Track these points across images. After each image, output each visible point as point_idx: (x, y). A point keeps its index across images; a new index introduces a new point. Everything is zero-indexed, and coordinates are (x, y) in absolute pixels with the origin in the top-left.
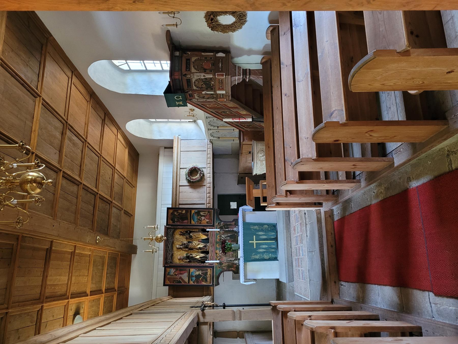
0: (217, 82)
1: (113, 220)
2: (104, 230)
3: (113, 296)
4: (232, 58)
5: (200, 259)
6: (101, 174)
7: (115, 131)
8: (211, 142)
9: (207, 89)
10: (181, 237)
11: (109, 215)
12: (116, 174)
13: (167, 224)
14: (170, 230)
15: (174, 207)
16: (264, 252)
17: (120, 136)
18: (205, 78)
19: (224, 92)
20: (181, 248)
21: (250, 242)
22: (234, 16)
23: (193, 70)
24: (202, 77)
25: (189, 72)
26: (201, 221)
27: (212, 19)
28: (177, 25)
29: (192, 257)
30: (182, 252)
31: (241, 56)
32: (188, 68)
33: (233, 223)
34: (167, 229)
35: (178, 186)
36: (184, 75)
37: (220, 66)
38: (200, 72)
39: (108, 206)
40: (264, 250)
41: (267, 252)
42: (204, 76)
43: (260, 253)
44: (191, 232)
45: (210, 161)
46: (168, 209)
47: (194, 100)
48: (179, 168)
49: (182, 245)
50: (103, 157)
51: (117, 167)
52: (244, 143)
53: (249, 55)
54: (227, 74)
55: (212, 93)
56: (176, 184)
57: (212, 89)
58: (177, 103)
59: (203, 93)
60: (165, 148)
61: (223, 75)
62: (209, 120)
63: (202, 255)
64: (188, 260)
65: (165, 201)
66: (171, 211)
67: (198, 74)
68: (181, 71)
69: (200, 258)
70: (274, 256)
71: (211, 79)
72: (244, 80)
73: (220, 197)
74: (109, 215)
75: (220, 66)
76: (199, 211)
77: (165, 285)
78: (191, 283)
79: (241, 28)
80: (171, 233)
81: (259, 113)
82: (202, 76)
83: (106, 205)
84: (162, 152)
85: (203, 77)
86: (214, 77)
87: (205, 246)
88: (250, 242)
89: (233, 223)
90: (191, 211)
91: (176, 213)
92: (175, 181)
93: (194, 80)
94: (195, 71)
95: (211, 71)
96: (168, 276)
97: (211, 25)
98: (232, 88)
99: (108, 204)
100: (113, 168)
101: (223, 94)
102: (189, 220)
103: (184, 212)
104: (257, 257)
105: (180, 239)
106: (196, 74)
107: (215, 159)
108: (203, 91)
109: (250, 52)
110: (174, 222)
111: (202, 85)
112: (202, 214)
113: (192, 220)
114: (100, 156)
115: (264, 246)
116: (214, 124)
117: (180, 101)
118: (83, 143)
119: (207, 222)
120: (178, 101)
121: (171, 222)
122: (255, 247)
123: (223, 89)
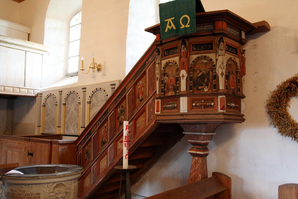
9: (189, 79)
42: (183, 76)
45: (8, 91)
58: (169, 20)
59: (183, 72)
62: (57, 95)
71: (216, 86)
82: (220, 71)
93: (212, 56)
95: (227, 87)
101: (178, 107)
108: (188, 72)
116: (70, 99)
120: (176, 22)
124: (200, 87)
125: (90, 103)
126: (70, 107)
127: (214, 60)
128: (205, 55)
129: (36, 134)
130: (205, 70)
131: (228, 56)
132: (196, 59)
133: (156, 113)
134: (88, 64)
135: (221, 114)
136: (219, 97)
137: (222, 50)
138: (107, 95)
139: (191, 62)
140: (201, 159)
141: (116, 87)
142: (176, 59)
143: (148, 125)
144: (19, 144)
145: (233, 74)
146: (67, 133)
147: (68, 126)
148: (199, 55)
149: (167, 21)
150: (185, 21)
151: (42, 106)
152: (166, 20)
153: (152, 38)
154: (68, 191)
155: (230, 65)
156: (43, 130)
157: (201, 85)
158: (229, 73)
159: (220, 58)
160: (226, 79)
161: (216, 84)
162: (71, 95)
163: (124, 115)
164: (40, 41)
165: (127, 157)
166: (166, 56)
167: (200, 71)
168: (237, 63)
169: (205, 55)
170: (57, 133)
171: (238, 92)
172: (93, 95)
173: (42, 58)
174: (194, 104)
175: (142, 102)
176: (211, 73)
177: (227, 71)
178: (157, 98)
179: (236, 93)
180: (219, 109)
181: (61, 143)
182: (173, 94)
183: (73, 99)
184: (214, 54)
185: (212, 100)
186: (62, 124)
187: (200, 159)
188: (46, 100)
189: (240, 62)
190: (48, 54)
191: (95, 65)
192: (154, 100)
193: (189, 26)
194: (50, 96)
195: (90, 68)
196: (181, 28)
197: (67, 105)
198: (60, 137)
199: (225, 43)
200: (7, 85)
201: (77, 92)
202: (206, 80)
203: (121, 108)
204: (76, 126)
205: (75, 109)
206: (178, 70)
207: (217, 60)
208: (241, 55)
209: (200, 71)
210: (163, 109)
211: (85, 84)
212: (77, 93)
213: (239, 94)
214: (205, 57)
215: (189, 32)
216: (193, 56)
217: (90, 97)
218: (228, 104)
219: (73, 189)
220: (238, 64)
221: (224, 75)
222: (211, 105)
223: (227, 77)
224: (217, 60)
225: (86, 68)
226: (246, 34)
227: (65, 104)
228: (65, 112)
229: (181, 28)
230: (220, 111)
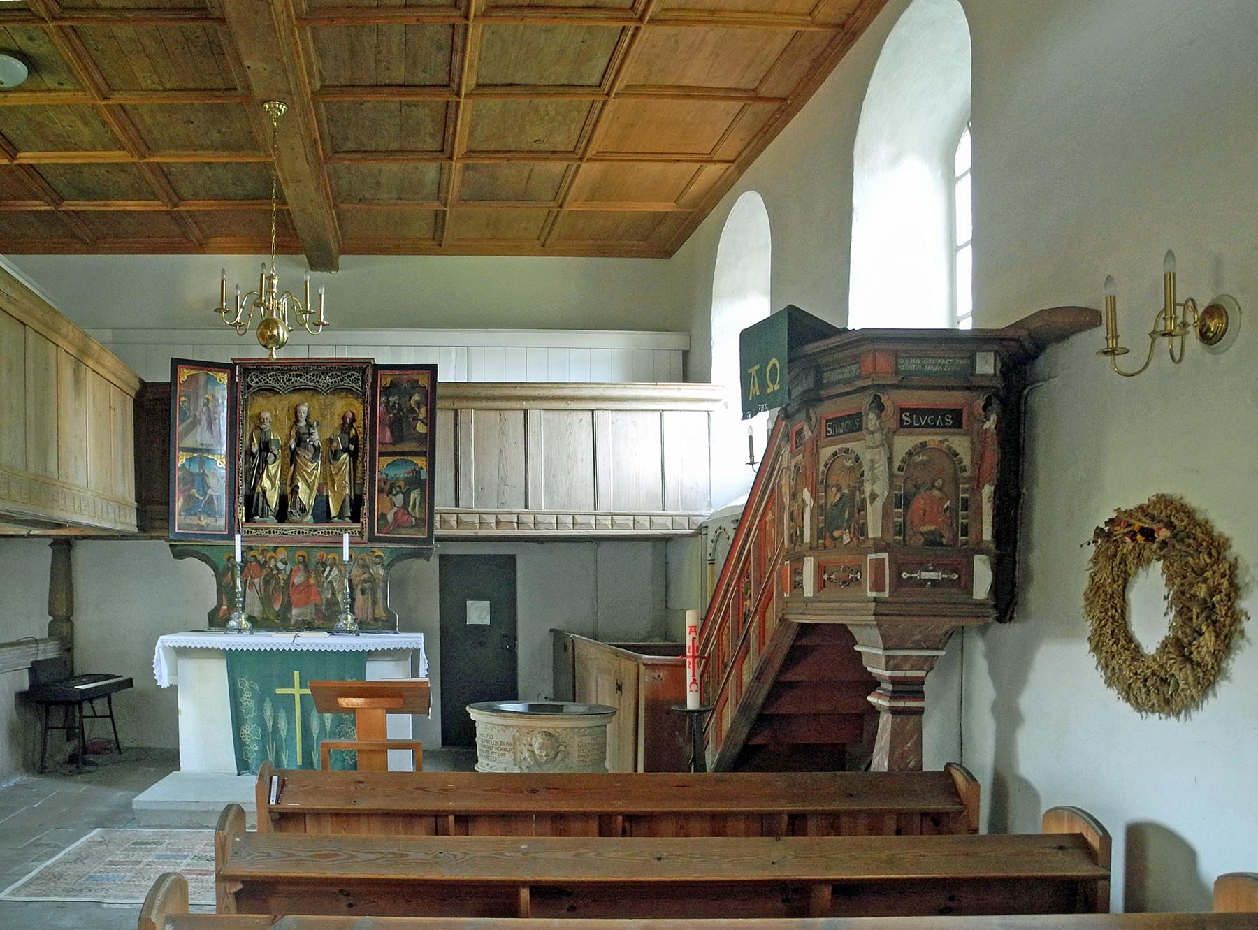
0: (848, 558)
1: (391, 168)
2: (346, 139)
3: (155, 197)
4: (984, 630)
5: (259, 489)
6: (537, 101)
7: (730, 148)
9: (819, 510)
10: (338, 422)
11: (401, 151)
12: (565, 164)
13: (377, 368)
14: (361, 376)
15: (439, 391)
16: (263, 725)
17: (712, 171)
18: (863, 500)
20: (297, 421)
21: (297, 674)
22: (1165, 645)
23: (904, 443)
24: (868, 489)
25: (892, 424)
26: (390, 492)
27: (1149, 535)
28: (1111, 352)
29: (266, 462)
30: (287, 423)
32: (914, 418)
33: (380, 613)
34: (365, 369)
35: (525, 405)
36: (877, 398)
37: (926, 575)
38: (892, 476)
39: (432, 144)
40: (269, 725)
41: (270, 736)
42: (874, 497)
43: (260, 709)
44: (354, 455)
45: (622, 527)
46: (432, 369)
48: (593, 406)
49: (309, 425)
50: (605, 103)
51: (590, 171)
53: (995, 708)
54: (882, 609)
56: (534, 398)
57: (820, 533)
58: (753, 371)
59: (806, 494)
60: (686, 354)
61: (878, 586)
63: (273, 499)
64: (255, 448)
65: (459, 360)
66: (423, 380)
67: (881, 468)
68: (898, 387)
69: (264, 492)
70: (253, 758)
71: (862, 530)
72: (872, 684)
73: (509, 563)
74: (401, 151)
75: (926, 575)
76: (427, 486)
77: (176, 363)
78: (182, 459)
79: (1109, 683)
80: (348, 383)
81: (749, 738)
83: (433, 136)
84: (672, 340)
85: (867, 494)
86: (870, 544)
87: (303, 510)
88: (297, 674)
89: (380, 613)
90: (423, 454)
91: (416, 397)
93: (856, 446)
94: (899, 455)
96: (202, 379)
97: (1119, 530)
98: (843, 629)
99: (439, 139)
100: (577, 153)
102: (390, 449)
103: (421, 428)
104: (247, 701)
105: (328, 415)
106: (881, 457)
107: (649, 544)
108: (814, 493)
109: (1008, 718)
110: (387, 391)
111: (839, 490)
112: (415, 495)
113: (391, 459)
114: (603, 89)
115: (283, 725)
117: (763, 386)
118: (632, 8)
119: (383, 516)
120: (761, 374)
121: (385, 380)
122: (279, 691)
123: (820, 585)
124: (836, 534)
139: (822, 468)
190: (726, 405)
196: (769, 391)
209: (839, 490)
210: (898, 583)
214: (847, 451)
218: (905, 575)
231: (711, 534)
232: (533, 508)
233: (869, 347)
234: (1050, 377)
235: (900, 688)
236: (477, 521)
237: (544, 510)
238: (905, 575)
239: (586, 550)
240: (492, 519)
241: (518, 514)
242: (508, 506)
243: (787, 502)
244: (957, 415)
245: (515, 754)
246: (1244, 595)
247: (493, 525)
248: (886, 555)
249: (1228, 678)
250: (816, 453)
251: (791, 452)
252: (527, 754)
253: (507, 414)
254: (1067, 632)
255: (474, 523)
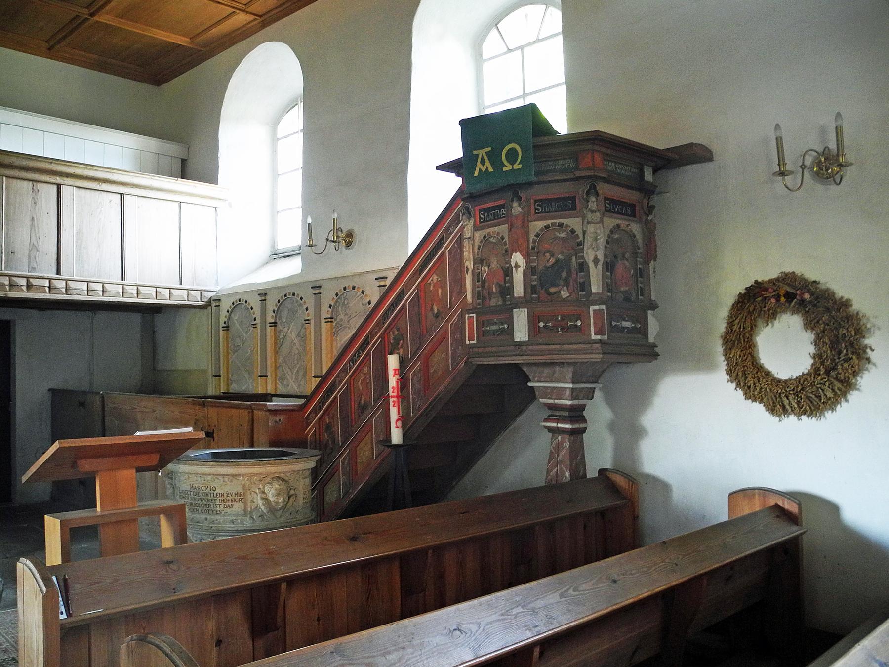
8: (209, 304)
9: (530, 271)
17: (241, 18)
19: (521, 334)
24: (589, 255)
31: (610, 400)
35: (58, 180)
42: (517, 266)
47: (468, 227)
52: (259, 414)
53: (613, 427)
55: (519, 290)
57: (530, 288)
58: (482, 152)
59: (517, 258)
62: (255, 302)
71: (584, 286)
82: (594, 253)
84: (172, 148)
92: (79, 171)
93: (574, 223)
95: (609, 287)
98: (516, 366)
101: (510, 332)
107: (136, 318)
108: (526, 257)
109: (629, 433)
116: (285, 313)
120: (494, 157)
124: (552, 290)
125: (330, 320)
126: (286, 329)
127: (579, 232)
128: (561, 221)
129: (211, 392)
130: (562, 253)
131: (611, 222)
132: (542, 230)
133: (468, 342)
134: (322, 234)
135: (595, 342)
136: (592, 308)
137: (592, 212)
138: (369, 303)
139: (532, 237)
140: (569, 440)
141: (388, 282)
142: (503, 229)
143: (453, 369)
144: (180, 412)
145: (627, 260)
146: (281, 390)
147: (284, 374)
148: (549, 222)
149: (478, 155)
150: (512, 156)
151: (221, 329)
152: (475, 152)
153: (453, 182)
154: (292, 492)
155: (618, 241)
156: (228, 385)
157: (556, 285)
158: (616, 257)
159: (591, 229)
160: (607, 271)
161: (584, 282)
162: (288, 304)
163: (402, 347)
164: (210, 176)
165: (399, 424)
166: (484, 222)
167: (552, 255)
168: (635, 236)
169: (561, 221)
170: (260, 390)
171: (640, 297)
172: (337, 301)
173: (217, 215)
174: (542, 324)
175: (439, 319)
176: (574, 258)
177: (608, 253)
178: (469, 311)
179: (633, 298)
180: (593, 334)
181: (273, 408)
182: (500, 303)
183: (293, 312)
184: (579, 220)
185: (579, 317)
186: (269, 367)
187: (567, 440)
188: (230, 315)
189: (643, 233)
190: (230, 205)
191: (341, 235)
192: (462, 316)
193: (520, 166)
194: (239, 304)
195: (327, 239)
197: (279, 327)
198: (267, 397)
199: (601, 197)
200: (143, 283)
201: (301, 295)
202: (564, 274)
203: (396, 333)
204: (301, 373)
205: (298, 335)
206: (508, 254)
207: (584, 233)
208: (644, 218)
209: (552, 255)
210: (612, 329)
211: (320, 273)
212: (301, 299)
213: (642, 301)
214: (561, 225)
215: (522, 179)
216: (536, 223)
217: (330, 307)
218: (614, 323)
219: (301, 488)
220: (639, 237)
221: (600, 264)
222: (576, 326)
223: (609, 267)
224: (584, 233)
225: (321, 243)
226: (655, 171)
227: (275, 323)
228: (275, 343)
229: (505, 169)
230: (594, 337)
231: (226, 305)
232: (65, 273)
233: (588, 147)
234: (660, 193)
235: (574, 414)
236: (7, 283)
237: (75, 278)
238: (614, 323)
239: (83, 317)
240: (23, 282)
241: (50, 279)
242: (40, 271)
243: (469, 264)
244: (633, 206)
245: (245, 504)
246: (867, 336)
247: (24, 288)
248: (604, 307)
249: (858, 389)
250: (525, 227)
251: (474, 225)
252: (260, 502)
253: (40, 186)
254: (702, 363)
255: (3, 285)
